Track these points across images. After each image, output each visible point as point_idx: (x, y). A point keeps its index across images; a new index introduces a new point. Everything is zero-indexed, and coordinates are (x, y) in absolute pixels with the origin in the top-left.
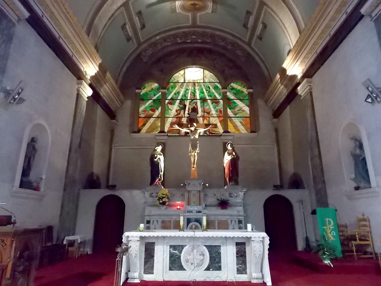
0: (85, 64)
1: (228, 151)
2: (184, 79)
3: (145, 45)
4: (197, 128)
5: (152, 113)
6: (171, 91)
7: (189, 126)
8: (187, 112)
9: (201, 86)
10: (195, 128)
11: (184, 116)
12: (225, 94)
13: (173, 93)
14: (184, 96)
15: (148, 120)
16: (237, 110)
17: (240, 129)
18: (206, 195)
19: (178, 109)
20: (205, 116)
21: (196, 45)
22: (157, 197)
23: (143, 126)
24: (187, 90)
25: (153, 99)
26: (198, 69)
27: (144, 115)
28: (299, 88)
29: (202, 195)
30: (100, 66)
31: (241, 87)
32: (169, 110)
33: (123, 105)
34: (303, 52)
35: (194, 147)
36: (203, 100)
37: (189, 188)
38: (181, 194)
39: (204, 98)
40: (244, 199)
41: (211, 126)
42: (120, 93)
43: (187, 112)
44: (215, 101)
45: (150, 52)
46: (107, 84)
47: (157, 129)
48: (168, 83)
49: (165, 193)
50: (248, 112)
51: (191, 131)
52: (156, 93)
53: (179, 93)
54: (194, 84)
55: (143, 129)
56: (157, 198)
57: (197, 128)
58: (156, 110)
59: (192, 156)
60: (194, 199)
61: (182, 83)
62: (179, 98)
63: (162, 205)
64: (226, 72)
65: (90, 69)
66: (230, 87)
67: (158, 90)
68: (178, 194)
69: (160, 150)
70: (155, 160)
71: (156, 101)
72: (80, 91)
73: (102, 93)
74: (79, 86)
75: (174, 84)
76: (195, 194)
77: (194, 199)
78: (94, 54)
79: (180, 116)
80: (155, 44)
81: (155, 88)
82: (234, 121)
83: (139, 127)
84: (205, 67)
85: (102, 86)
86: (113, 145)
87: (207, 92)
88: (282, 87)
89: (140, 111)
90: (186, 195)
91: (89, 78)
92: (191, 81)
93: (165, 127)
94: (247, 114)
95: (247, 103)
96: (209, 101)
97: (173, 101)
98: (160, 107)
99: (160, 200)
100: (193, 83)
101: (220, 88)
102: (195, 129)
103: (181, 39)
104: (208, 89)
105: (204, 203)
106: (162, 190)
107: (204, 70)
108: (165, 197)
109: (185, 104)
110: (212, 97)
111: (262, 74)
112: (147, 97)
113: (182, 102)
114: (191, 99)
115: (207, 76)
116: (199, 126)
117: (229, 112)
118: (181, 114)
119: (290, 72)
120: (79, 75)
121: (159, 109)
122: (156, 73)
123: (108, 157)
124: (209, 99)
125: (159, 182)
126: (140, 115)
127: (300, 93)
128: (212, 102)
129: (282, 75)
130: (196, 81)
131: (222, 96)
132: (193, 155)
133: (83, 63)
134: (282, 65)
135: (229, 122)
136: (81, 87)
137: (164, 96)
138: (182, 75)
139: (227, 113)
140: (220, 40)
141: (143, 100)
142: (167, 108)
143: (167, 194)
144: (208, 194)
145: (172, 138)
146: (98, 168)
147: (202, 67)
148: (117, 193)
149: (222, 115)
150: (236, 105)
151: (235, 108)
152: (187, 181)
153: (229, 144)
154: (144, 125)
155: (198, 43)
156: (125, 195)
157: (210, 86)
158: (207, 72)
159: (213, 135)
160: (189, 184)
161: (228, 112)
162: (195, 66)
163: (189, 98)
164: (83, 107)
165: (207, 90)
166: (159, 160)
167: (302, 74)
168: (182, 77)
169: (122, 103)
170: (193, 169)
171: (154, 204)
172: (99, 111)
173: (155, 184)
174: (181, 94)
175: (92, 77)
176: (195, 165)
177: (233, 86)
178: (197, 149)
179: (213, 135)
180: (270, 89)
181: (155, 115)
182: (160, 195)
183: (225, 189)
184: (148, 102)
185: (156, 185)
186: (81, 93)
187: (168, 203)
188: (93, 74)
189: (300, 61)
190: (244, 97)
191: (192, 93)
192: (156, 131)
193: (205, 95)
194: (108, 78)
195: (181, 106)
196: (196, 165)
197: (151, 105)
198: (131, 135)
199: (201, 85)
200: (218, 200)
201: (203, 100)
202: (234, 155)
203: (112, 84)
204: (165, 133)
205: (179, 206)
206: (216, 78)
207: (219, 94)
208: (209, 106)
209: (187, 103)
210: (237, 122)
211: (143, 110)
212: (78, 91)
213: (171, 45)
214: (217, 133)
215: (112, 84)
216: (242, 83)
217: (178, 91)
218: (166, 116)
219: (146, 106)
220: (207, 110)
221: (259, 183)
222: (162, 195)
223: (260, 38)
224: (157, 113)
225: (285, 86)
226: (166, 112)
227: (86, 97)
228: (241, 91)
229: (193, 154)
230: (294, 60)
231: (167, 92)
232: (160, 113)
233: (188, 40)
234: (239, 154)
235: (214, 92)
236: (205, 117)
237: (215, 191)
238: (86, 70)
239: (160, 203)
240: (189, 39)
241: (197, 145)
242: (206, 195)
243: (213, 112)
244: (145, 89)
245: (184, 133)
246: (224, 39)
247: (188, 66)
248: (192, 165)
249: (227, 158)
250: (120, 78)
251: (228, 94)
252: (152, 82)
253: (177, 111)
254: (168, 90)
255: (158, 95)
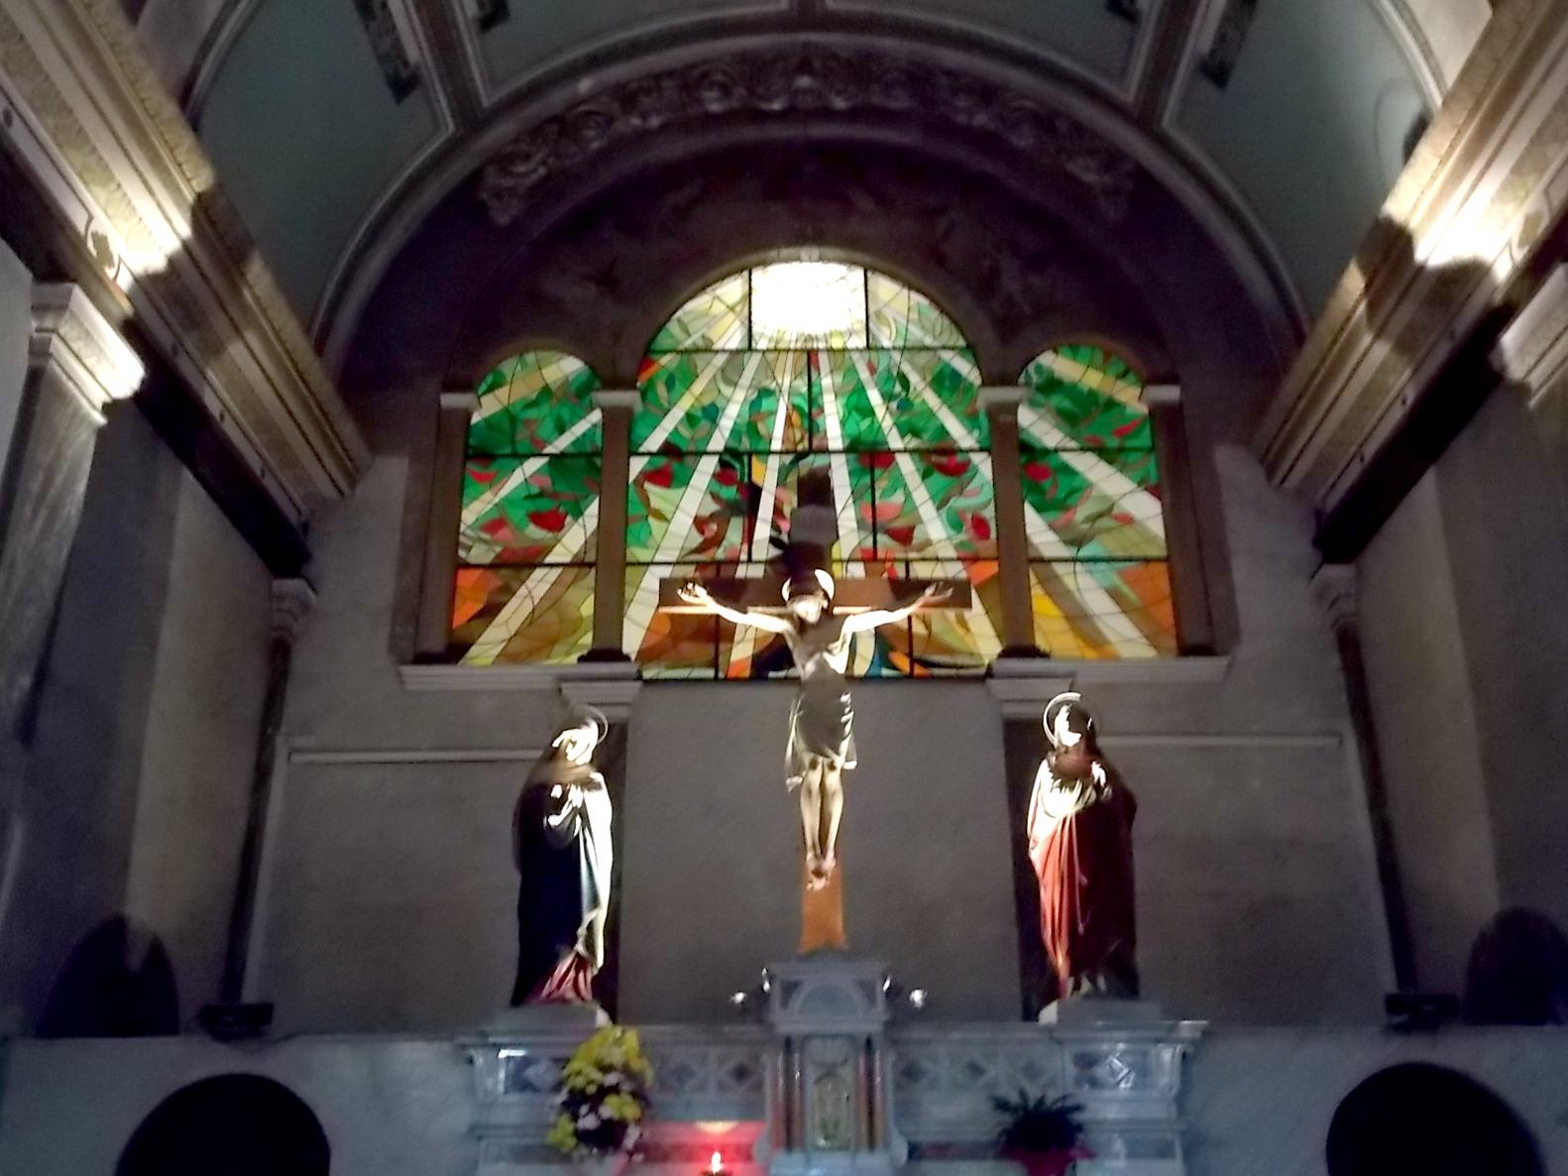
0: (98, 190)
1: (1053, 759)
2: (746, 331)
3: (501, 132)
4: (837, 610)
5: (542, 539)
6: (666, 404)
7: (786, 593)
8: (763, 531)
9: (853, 369)
10: (825, 604)
11: (744, 557)
12: (1004, 418)
13: (677, 414)
14: (744, 429)
15: (514, 585)
16: (1081, 513)
17: (1112, 637)
18: (910, 1073)
19: (706, 512)
20: (881, 554)
21: (820, 131)
22: (557, 1087)
23: (479, 622)
24: (765, 392)
25: (549, 450)
26: (836, 270)
27: (488, 551)
28: (1510, 338)
29: (885, 1065)
30: (203, 212)
31: (1104, 372)
32: (651, 520)
33: (359, 490)
34: (1533, 95)
35: (822, 734)
36: (870, 456)
37: (789, 1021)
38: (731, 1065)
39: (875, 443)
40: (1181, 1100)
41: (929, 591)
42: (335, 406)
43: (763, 531)
44: (944, 460)
45: (531, 171)
46: (252, 338)
47: (571, 640)
48: (646, 358)
49: (616, 1057)
50: (1157, 527)
51: (801, 625)
52: (566, 414)
53: (712, 413)
54: (810, 357)
55: (481, 640)
56: (562, 1097)
57: (837, 610)
58: (569, 519)
59: (810, 792)
60: (828, 1102)
61: (731, 352)
62: (718, 443)
63: (595, 1150)
64: (1011, 282)
65: (136, 225)
66: (1035, 379)
67: (578, 396)
68: (712, 1061)
69: (588, 757)
70: (554, 820)
71: (568, 461)
72: (51, 355)
73: (216, 393)
74: (48, 323)
75: (681, 360)
76: (835, 1065)
77: (828, 1102)
78: (163, 128)
79: (720, 554)
80: (565, 125)
81: (566, 383)
82: (1069, 581)
83: (455, 624)
84: (875, 254)
85: (216, 349)
86: (280, 740)
87: (894, 405)
88: (1382, 351)
89: (462, 528)
90: (772, 1064)
91: (125, 282)
92: (790, 339)
93: (626, 621)
94: (1150, 539)
95: (1148, 473)
96: (906, 465)
97: (675, 466)
98: (596, 502)
99: (584, 1109)
100: (804, 357)
101: (971, 385)
102: (826, 613)
103: (726, 91)
104: (898, 388)
105: (902, 1133)
106: (597, 1039)
107: (869, 274)
108: (615, 1090)
109: (756, 478)
110: (926, 436)
111: (1233, 289)
112: (513, 442)
113: (733, 467)
114: (787, 452)
115: (888, 313)
116: (847, 594)
117: (1037, 528)
118: (724, 543)
119: (1433, 250)
120: (55, 259)
121: (587, 512)
122: (571, 289)
123: (241, 823)
124: (905, 451)
125: (576, 979)
126: (462, 553)
127: (1516, 370)
128: (922, 466)
129: (1376, 272)
130: (817, 339)
131: (986, 430)
132: (816, 786)
133: (85, 183)
134: (1384, 198)
135: (1037, 591)
136: (62, 331)
137: (620, 430)
138: (732, 309)
139: (1026, 538)
140: (962, 102)
141: (486, 457)
142: (635, 508)
143: (637, 1064)
144: (926, 1064)
145: (674, 695)
146: (161, 887)
147: (858, 256)
148: (276, 1064)
149: (989, 546)
150: (1076, 483)
151: (1070, 501)
152: (777, 968)
153: (1064, 713)
154: (489, 612)
155: (827, 114)
156: (328, 1076)
157: (906, 368)
158: (886, 289)
159: (937, 671)
160: (790, 989)
161: (1029, 530)
162: (815, 252)
163: (776, 445)
164: (65, 465)
165: (888, 397)
166: (578, 820)
167: (1521, 244)
168: (731, 317)
169: (353, 475)
170: (819, 884)
171: (537, 1141)
172: (191, 511)
173: (545, 992)
174: (726, 423)
175: (148, 285)
176: (830, 854)
177: (1051, 372)
178: (845, 746)
179: (933, 678)
180: (1291, 386)
181: (558, 549)
182: (579, 1073)
183: (1049, 1029)
184: (518, 471)
185: (555, 1000)
186: (58, 370)
187: (641, 1135)
188: (157, 263)
189: (1512, 162)
190: (1122, 433)
191: (795, 418)
192: (568, 654)
193: (876, 425)
194: (257, 299)
195: (730, 493)
196: (835, 856)
197: (535, 490)
198: (400, 675)
199: (854, 366)
200: (1002, 1105)
201: (870, 456)
202: (1098, 787)
203: (282, 343)
204: (627, 658)
205: (716, 1157)
206: (947, 322)
207: (970, 418)
208: (908, 495)
209: (766, 474)
210: (1090, 589)
211: (481, 522)
212: (40, 351)
213: (664, 128)
214: (960, 660)
215: (282, 343)
216: (1107, 355)
217: (706, 402)
218: (629, 558)
219: (503, 493)
220: (892, 520)
221: (1261, 985)
222: (597, 1076)
223: (1216, 71)
224: (574, 539)
225: (1404, 345)
226: (633, 528)
227: (90, 402)
228: (1102, 400)
229: (815, 777)
230: (1469, 157)
231: (639, 408)
232: (593, 542)
233: (769, 100)
234: (1131, 784)
235: (935, 409)
236: (885, 561)
237: (964, 1041)
238: (102, 224)
239: (582, 1136)
240: (777, 96)
241: (844, 719)
242: (910, 1073)
243: (935, 528)
244: (502, 393)
245: (749, 662)
246: (987, 93)
247: (773, 254)
248: (810, 855)
249: (1053, 808)
250: (347, 320)
251: (1025, 417)
252: (543, 348)
253: (700, 523)
254: (644, 396)
255: (580, 428)
